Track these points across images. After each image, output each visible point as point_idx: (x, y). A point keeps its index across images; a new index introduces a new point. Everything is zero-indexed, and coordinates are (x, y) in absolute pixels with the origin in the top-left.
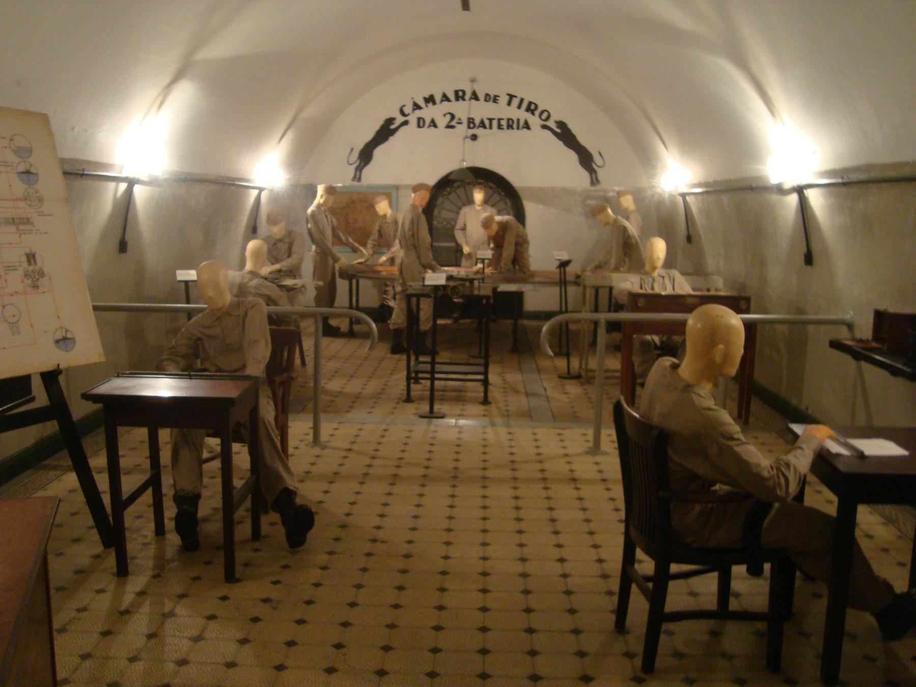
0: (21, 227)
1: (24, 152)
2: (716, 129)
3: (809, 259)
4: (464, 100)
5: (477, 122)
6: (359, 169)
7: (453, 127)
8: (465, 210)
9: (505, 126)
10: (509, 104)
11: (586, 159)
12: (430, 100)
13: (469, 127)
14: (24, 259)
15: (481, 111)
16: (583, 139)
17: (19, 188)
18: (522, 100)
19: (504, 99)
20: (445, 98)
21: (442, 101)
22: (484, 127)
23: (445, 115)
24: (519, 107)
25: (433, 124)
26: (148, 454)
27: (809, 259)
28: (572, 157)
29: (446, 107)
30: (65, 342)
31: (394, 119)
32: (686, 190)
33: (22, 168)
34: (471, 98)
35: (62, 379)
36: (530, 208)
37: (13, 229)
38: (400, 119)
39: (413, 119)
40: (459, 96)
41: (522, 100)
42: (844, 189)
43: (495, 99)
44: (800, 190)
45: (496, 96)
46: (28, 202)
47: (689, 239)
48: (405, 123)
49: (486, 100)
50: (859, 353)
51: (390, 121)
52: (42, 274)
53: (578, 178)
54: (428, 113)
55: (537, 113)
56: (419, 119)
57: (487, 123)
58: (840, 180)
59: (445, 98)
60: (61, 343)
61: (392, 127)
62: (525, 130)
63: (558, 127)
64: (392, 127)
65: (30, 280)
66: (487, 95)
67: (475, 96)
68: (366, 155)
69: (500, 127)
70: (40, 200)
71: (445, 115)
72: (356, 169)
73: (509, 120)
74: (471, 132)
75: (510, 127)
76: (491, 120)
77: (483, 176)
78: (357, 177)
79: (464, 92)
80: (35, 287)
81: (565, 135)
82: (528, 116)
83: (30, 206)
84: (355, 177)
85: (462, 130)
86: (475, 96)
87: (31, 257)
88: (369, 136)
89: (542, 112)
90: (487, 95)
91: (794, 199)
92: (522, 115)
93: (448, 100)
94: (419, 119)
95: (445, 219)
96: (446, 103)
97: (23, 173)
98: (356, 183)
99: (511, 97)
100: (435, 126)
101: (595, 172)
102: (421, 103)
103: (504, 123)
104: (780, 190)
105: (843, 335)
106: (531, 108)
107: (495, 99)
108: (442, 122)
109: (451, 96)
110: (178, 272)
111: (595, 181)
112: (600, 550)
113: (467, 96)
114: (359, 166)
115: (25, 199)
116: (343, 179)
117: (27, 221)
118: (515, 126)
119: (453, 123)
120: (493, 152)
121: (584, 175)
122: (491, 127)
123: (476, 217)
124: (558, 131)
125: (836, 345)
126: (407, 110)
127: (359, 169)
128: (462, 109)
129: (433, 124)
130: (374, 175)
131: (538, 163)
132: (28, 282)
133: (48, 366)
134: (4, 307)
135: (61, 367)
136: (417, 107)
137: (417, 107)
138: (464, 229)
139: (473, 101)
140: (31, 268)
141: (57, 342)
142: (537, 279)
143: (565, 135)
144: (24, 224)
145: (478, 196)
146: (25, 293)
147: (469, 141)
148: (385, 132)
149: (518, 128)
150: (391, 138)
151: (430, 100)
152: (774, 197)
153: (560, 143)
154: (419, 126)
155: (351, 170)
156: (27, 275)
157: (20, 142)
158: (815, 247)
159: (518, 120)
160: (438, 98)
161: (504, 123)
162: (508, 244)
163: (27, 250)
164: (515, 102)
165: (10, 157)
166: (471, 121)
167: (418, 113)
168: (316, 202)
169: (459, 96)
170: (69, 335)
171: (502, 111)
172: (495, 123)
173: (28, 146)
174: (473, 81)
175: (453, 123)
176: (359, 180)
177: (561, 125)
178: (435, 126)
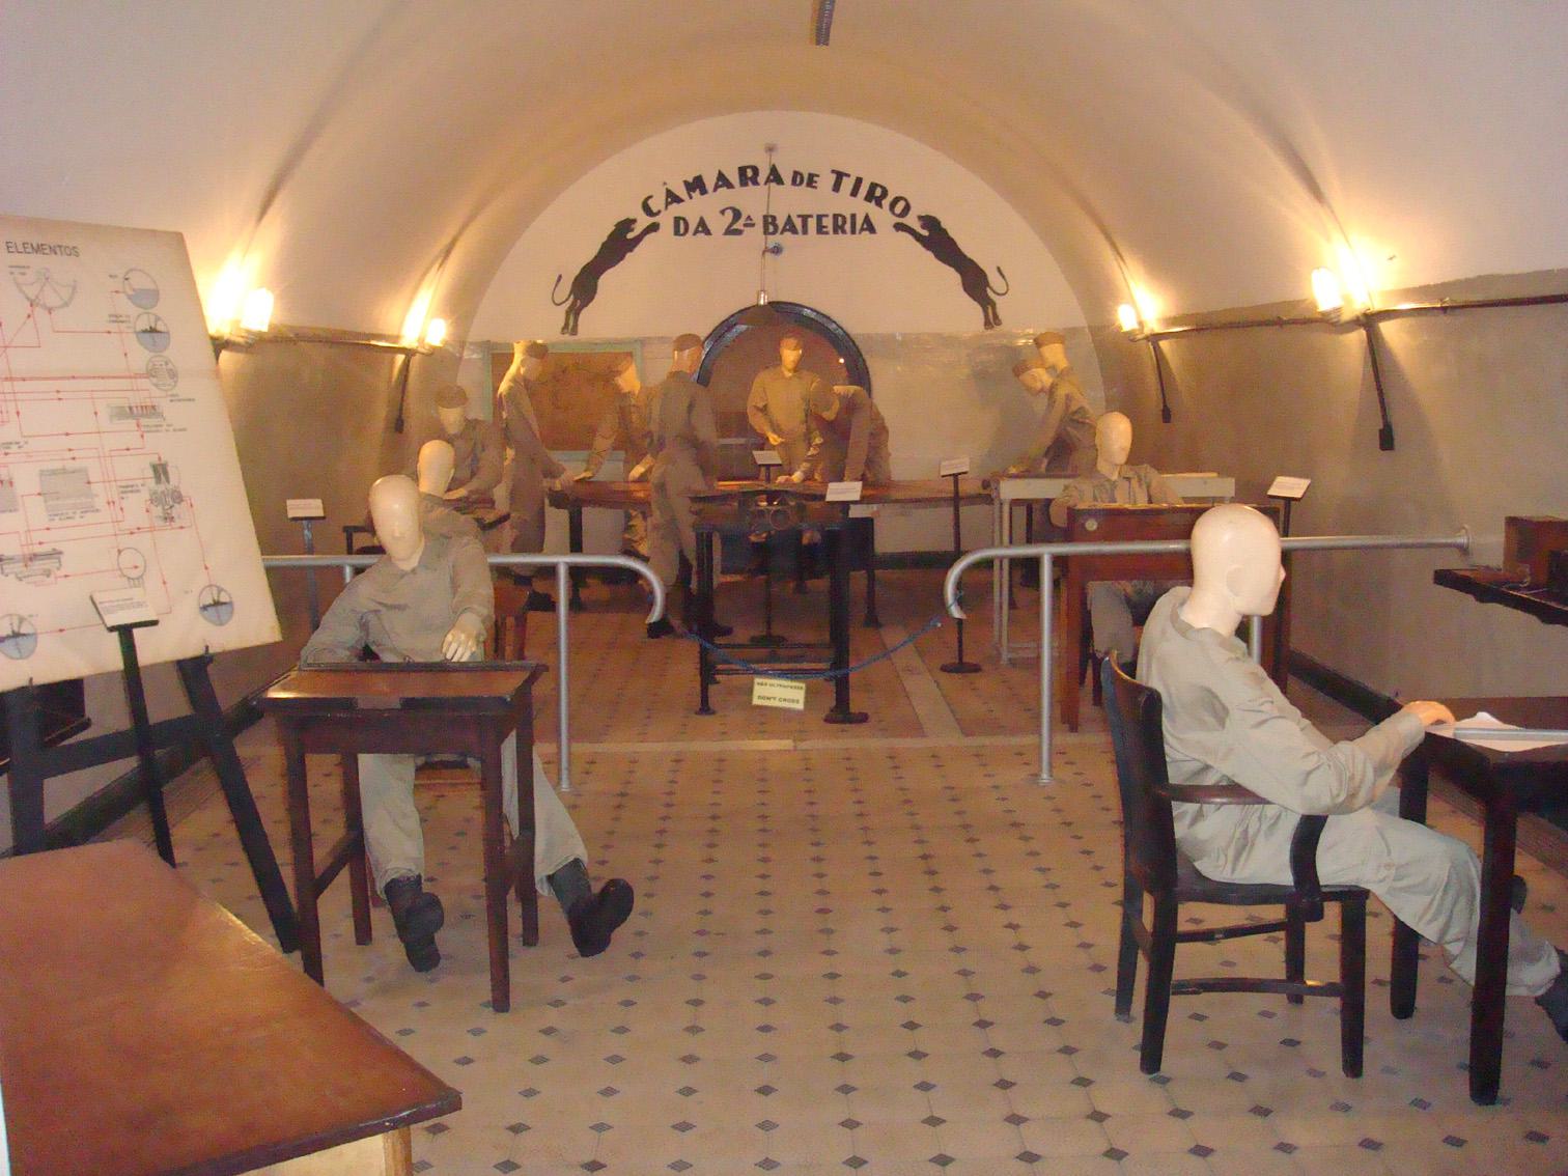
0: (144, 421)
1: (147, 298)
3: (1387, 440)
4: (756, 183)
5: (781, 223)
6: (574, 312)
7: (739, 232)
8: (763, 379)
9: (830, 229)
10: (836, 187)
11: (975, 281)
12: (696, 185)
13: (766, 232)
14: (150, 473)
15: (788, 201)
17: (140, 357)
18: (859, 181)
19: (826, 181)
20: (723, 181)
22: (794, 231)
23: (723, 212)
24: (854, 193)
25: (703, 228)
27: (1387, 440)
28: (952, 277)
31: (634, 221)
32: (1158, 329)
33: (143, 324)
34: (768, 181)
35: (210, 669)
36: (882, 373)
37: (132, 423)
38: (644, 221)
39: (666, 221)
40: (748, 176)
41: (859, 181)
42: (1444, 319)
43: (811, 181)
44: (1369, 322)
45: (811, 176)
46: (155, 380)
47: (1166, 415)
48: (654, 228)
49: (794, 182)
50: (1483, 588)
51: (626, 225)
52: (178, 498)
53: (966, 315)
54: (693, 208)
55: (886, 202)
56: (677, 220)
57: (798, 223)
58: (1194, 327)
59: (723, 181)
60: (211, 610)
61: (630, 236)
62: (701, 236)
63: (923, 227)
64: (630, 236)
65: (160, 508)
66: (796, 173)
67: (775, 177)
68: (585, 286)
69: (821, 229)
70: (173, 374)
71: (723, 212)
72: (568, 313)
73: (836, 217)
74: (773, 240)
75: (838, 228)
76: (805, 218)
77: (782, 317)
78: (570, 327)
79: (755, 170)
80: (169, 518)
81: (937, 240)
82: (871, 208)
83: (156, 385)
86: (775, 177)
87: (160, 471)
88: (589, 252)
89: (897, 200)
90: (796, 173)
91: (1358, 337)
92: (860, 207)
93: (729, 185)
94: (677, 220)
96: (723, 190)
97: (145, 331)
98: (567, 337)
100: (707, 232)
102: (681, 192)
103: (828, 222)
104: (1330, 323)
105: (1454, 563)
106: (876, 195)
107: (811, 181)
108: (718, 224)
109: (734, 178)
110: (290, 502)
111: (992, 320)
113: (762, 178)
115: (150, 374)
116: (547, 326)
118: (848, 227)
119: (738, 225)
120: (817, 276)
121: (975, 308)
122: (805, 232)
123: (783, 390)
124: (925, 233)
125: (1444, 578)
126: (657, 204)
127: (574, 312)
128: (753, 201)
129: (703, 228)
130: (604, 321)
131: (884, 293)
132: (158, 511)
133: (192, 650)
134: (120, 552)
135: (211, 651)
137: (672, 198)
138: (764, 410)
139: (773, 185)
141: (205, 608)
142: (899, 495)
143: (937, 240)
145: (790, 354)
146: (152, 529)
148: (619, 244)
149: (853, 232)
151: (696, 185)
152: (1322, 339)
153: (930, 255)
154: (677, 232)
155: (560, 314)
156: (155, 499)
157: (139, 282)
158: (1395, 418)
159: (853, 216)
160: (710, 182)
161: (828, 222)
162: (846, 433)
163: (155, 460)
164: (847, 184)
165: (126, 307)
166: (769, 222)
167: (676, 210)
168: (513, 370)
169: (748, 176)
170: (224, 598)
171: (825, 201)
172: (812, 223)
173: (152, 287)
174: (770, 149)
175: (738, 225)
176: (574, 332)
177: (930, 222)
178: (707, 232)
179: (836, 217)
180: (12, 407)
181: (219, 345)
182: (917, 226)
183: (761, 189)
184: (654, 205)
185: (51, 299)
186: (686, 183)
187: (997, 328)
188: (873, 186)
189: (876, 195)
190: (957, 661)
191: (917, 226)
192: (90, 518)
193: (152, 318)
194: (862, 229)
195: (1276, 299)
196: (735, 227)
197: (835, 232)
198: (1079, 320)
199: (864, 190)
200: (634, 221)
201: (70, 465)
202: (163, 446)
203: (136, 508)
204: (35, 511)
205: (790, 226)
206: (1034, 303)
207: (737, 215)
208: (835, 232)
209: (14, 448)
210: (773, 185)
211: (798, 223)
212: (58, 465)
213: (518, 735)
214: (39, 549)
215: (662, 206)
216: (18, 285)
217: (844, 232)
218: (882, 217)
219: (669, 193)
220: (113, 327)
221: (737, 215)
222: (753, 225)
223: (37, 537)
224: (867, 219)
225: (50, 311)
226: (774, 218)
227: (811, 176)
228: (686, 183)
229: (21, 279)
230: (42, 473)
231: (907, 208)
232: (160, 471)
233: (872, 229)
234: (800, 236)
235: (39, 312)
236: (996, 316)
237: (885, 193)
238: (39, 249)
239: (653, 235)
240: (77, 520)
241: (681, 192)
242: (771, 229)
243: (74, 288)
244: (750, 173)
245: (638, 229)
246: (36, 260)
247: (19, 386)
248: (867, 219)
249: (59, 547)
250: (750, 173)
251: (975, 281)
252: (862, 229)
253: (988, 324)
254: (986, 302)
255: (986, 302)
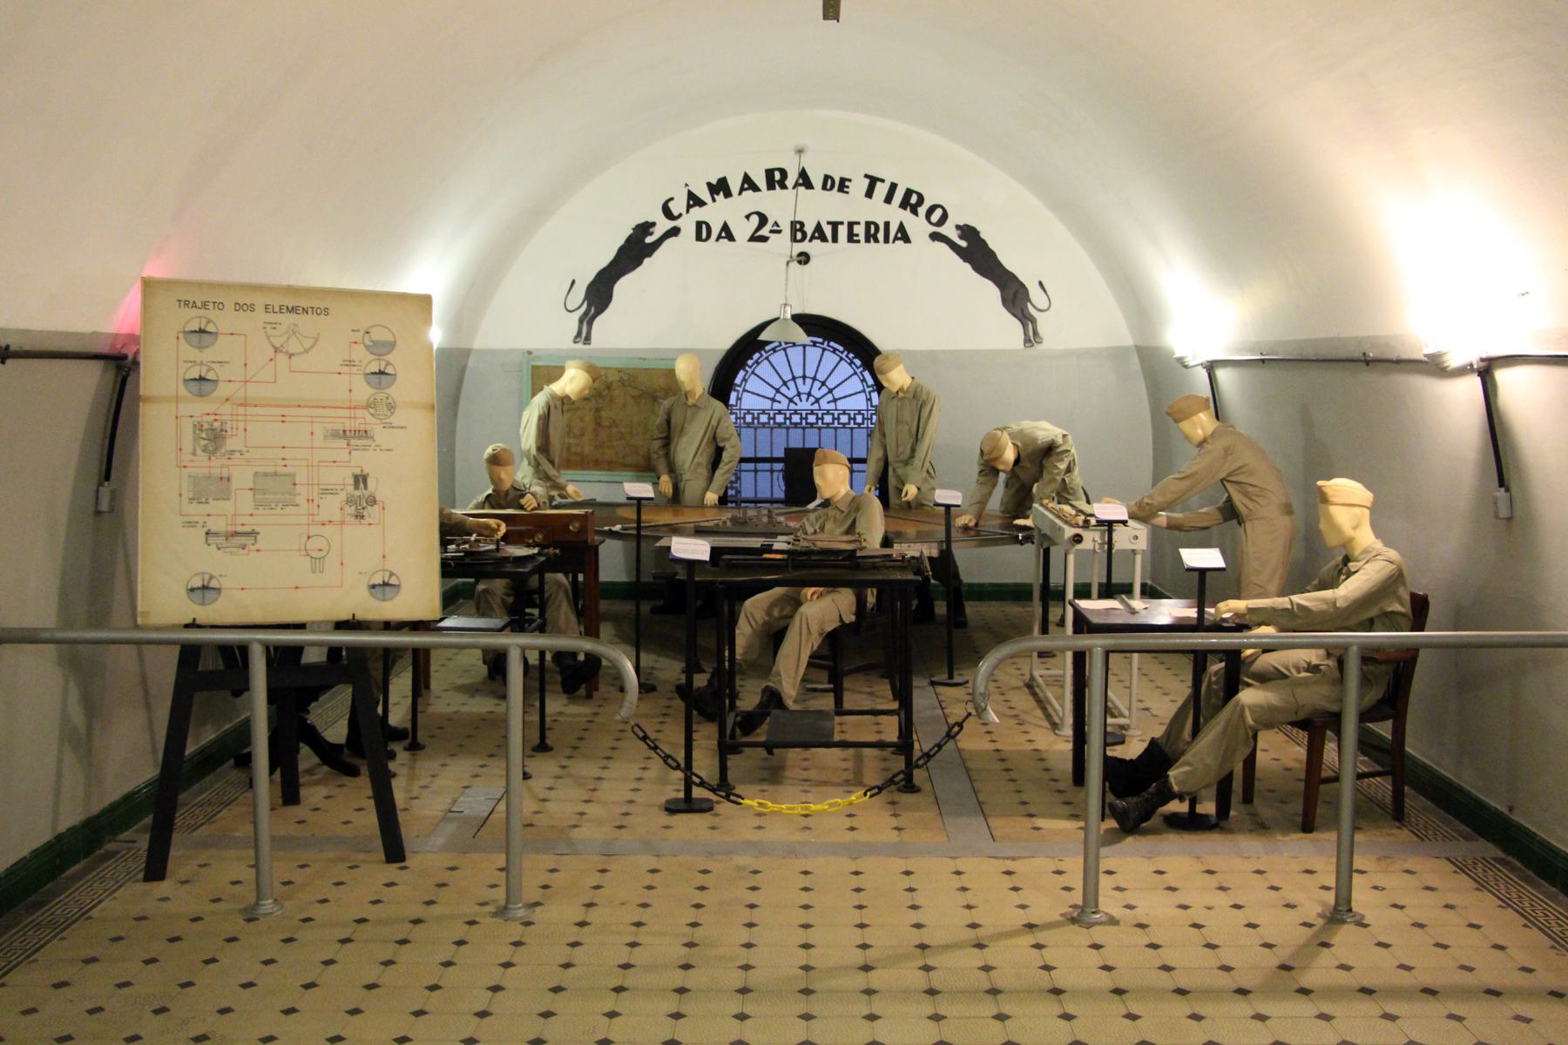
0: (353, 442)
1: (382, 348)
2: (1252, 204)
4: (784, 187)
5: (809, 229)
6: (588, 320)
7: (764, 239)
9: (862, 237)
10: (869, 193)
11: (1014, 294)
12: (720, 187)
13: (794, 240)
14: (351, 481)
15: (817, 207)
16: (1008, 259)
17: (363, 392)
18: (893, 187)
19: (858, 186)
20: (748, 184)
21: (742, 190)
22: (824, 239)
23: (748, 217)
24: (888, 199)
25: (727, 233)
26: (370, 793)
29: (751, 201)
30: (384, 588)
31: (653, 224)
34: (796, 185)
37: (342, 443)
38: (663, 225)
39: (687, 224)
40: (776, 179)
41: (893, 187)
43: (843, 186)
45: (843, 180)
48: (674, 232)
49: (824, 187)
51: (645, 228)
54: (715, 212)
55: (922, 210)
56: (699, 224)
57: (828, 230)
59: (748, 184)
61: (649, 240)
62: (899, 243)
63: (961, 237)
64: (649, 240)
66: (827, 177)
67: (805, 181)
68: (600, 293)
69: (851, 238)
71: (748, 217)
72: (581, 321)
73: (868, 224)
74: (799, 247)
75: (870, 237)
76: (835, 225)
79: (784, 173)
80: (359, 516)
81: (976, 252)
82: (906, 216)
84: (579, 334)
85: (781, 244)
86: (805, 181)
87: (360, 480)
92: (895, 215)
93: (755, 188)
95: (749, 412)
98: (580, 346)
99: (873, 181)
100: (731, 238)
101: (1033, 321)
102: (704, 194)
103: (860, 230)
106: (911, 202)
107: (843, 186)
108: (743, 229)
109: (761, 181)
111: (1032, 338)
112: (1060, 1012)
113: (790, 182)
114: (586, 314)
117: (365, 434)
118: (881, 236)
119: (764, 232)
120: (845, 285)
121: (1016, 324)
122: (835, 240)
124: (963, 244)
126: (677, 207)
127: (588, 320)
128: (780, 206)
129: (727, 233)
131: (918, 307)
132: (350, 510)
136: (694, 201)
137: (694, 201)
140: (357, 493)
143: (976, 252)
144: (360, 438)
147: (795, 265)
148: (636, 249)
150: (647, 261)
151: (720, 187)
154: (699, 238)
156: (350, 501)
157: (379, 335)
159: (887, 224)
160: (735, 186)
161: (860, 230)
163: (357, 471)
164: (881, 190)
165: (360, 354)
166: (797, 228)
167: (698, 213)
169: (776, 179)
170: (393, 581)
171: (855, 207)
172: (843, 231)
174: (800, 151)
175: (764, 232)
176: (588, 339)
177: (968, 232)
178: (731, 238)
179: (868, 224)
180: (241, 425)
181: (937, 505)
182: (953, 235)
183: (790, 193)
184: (675, 208)
185: (294, 347)
186: (709, 184)
187: (1038, 347)
188: (909, 192)
189: (911, 202)
190: (681, 795)
191: (953, 235)
192: (289, 509)
193: (383, 364)
194: (896, 238)
195: (1360, 333)
196: (760, 233)
197: (867, 241)
198: (1127, 340)
199: (898, 196)
200: (653, 224)
201: (281, 470)
202: (364, 460)
203: (332, 507)
204: (245, 502)
205: (819, 233)
206: (1079, 317)
207: (763, 220)
208: (867, 241)
209: (237, 455)
210: (802, 189)
211: (828, 230)
212: (270, 470)
213: (282, 775)
214: (240, 529)
215: (683, 211)
216: (268, 337)
217: (877, 241)
218: (918, 226)
219: (691, 196)
220: (346, 369)
221: (763, 220)
222: (779, 232)
223: (240, 520)
224: (901, 228)
225: (291, 356)
226: (802, 224)
227: (843, 180)
228: (709, 184)
229: (270, 332)
230: (256, 474)
231: (944, 217)
232: (360, 480)
233: (906, 239)
234: (830, 244)
235: (282, 358)
236: (1035, 333)
237: (921, 199)
238: (293, 310)
239: (673, 239)
240: (279, 510)
241: (704, 194)
242: (799, 236)
243: (316, 339)
244: (777, 176)
245: (658, 232)
246: (287, 319)
247: (250, 410)
248: (901, 228)
249: (257, 529)
250: (777, 176)
251: (1014, 294)
252: (896, 238)
253: (1027, 341)
254: (1025, 318)
255: (1025, 318)
